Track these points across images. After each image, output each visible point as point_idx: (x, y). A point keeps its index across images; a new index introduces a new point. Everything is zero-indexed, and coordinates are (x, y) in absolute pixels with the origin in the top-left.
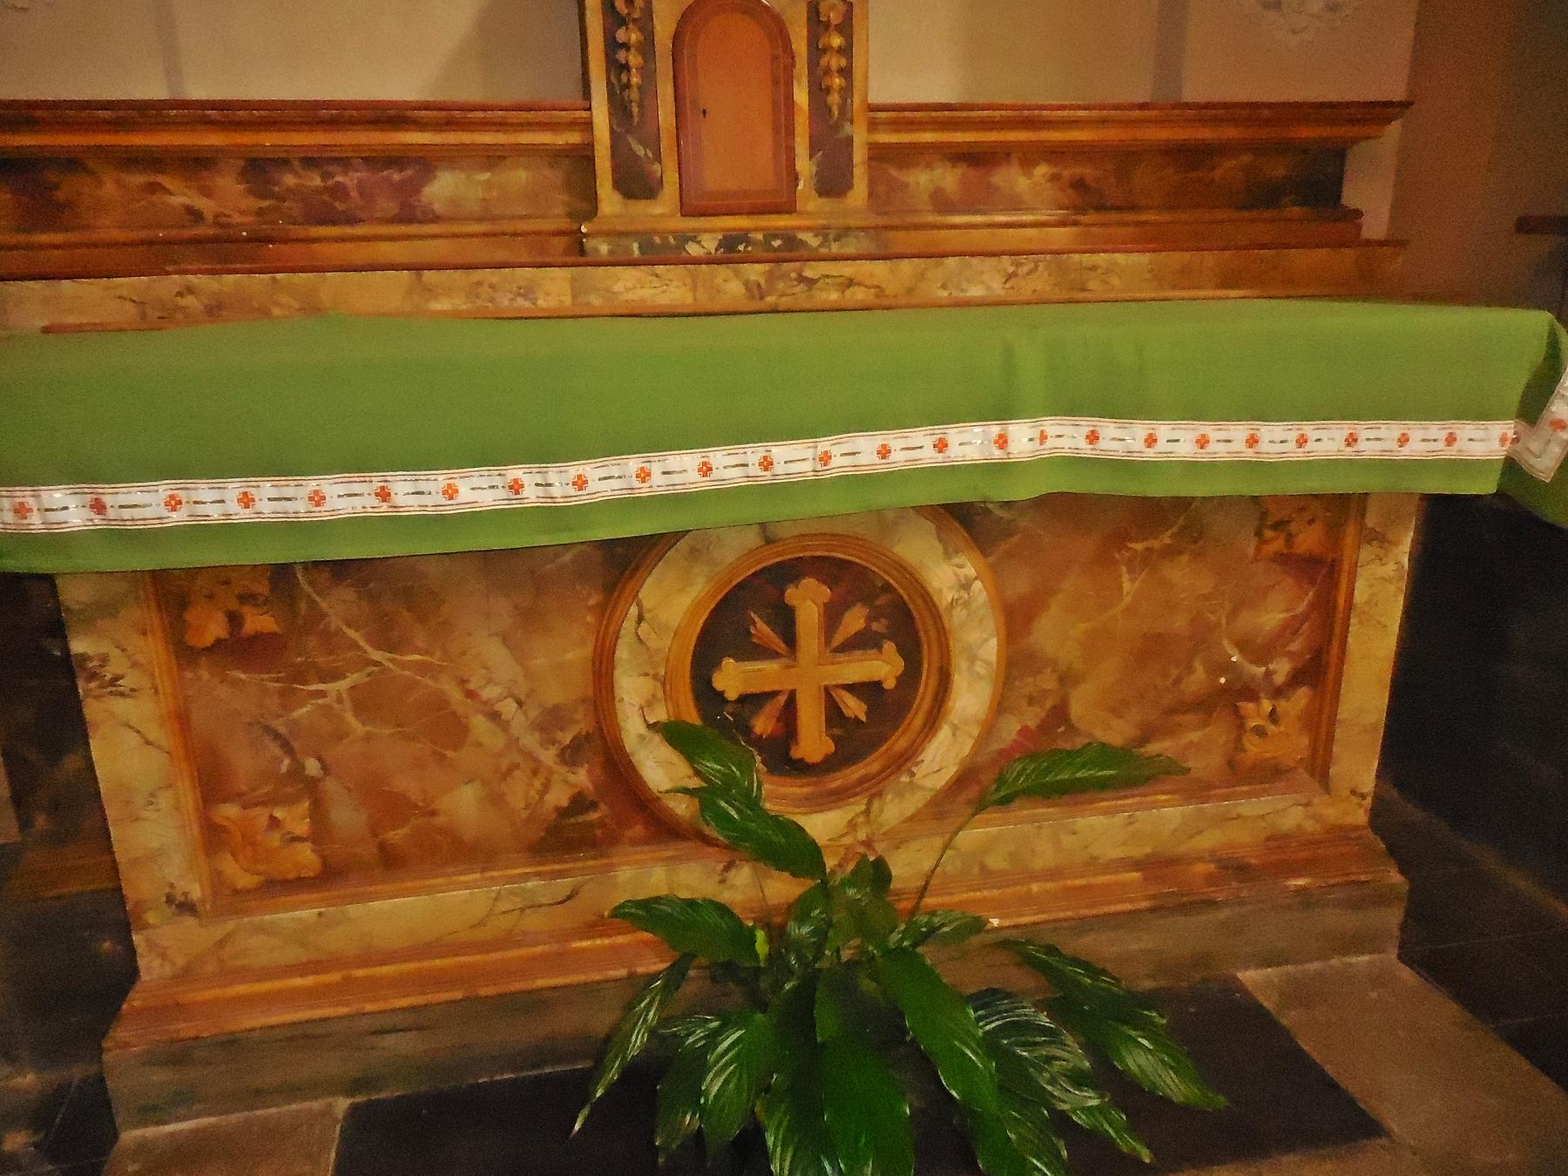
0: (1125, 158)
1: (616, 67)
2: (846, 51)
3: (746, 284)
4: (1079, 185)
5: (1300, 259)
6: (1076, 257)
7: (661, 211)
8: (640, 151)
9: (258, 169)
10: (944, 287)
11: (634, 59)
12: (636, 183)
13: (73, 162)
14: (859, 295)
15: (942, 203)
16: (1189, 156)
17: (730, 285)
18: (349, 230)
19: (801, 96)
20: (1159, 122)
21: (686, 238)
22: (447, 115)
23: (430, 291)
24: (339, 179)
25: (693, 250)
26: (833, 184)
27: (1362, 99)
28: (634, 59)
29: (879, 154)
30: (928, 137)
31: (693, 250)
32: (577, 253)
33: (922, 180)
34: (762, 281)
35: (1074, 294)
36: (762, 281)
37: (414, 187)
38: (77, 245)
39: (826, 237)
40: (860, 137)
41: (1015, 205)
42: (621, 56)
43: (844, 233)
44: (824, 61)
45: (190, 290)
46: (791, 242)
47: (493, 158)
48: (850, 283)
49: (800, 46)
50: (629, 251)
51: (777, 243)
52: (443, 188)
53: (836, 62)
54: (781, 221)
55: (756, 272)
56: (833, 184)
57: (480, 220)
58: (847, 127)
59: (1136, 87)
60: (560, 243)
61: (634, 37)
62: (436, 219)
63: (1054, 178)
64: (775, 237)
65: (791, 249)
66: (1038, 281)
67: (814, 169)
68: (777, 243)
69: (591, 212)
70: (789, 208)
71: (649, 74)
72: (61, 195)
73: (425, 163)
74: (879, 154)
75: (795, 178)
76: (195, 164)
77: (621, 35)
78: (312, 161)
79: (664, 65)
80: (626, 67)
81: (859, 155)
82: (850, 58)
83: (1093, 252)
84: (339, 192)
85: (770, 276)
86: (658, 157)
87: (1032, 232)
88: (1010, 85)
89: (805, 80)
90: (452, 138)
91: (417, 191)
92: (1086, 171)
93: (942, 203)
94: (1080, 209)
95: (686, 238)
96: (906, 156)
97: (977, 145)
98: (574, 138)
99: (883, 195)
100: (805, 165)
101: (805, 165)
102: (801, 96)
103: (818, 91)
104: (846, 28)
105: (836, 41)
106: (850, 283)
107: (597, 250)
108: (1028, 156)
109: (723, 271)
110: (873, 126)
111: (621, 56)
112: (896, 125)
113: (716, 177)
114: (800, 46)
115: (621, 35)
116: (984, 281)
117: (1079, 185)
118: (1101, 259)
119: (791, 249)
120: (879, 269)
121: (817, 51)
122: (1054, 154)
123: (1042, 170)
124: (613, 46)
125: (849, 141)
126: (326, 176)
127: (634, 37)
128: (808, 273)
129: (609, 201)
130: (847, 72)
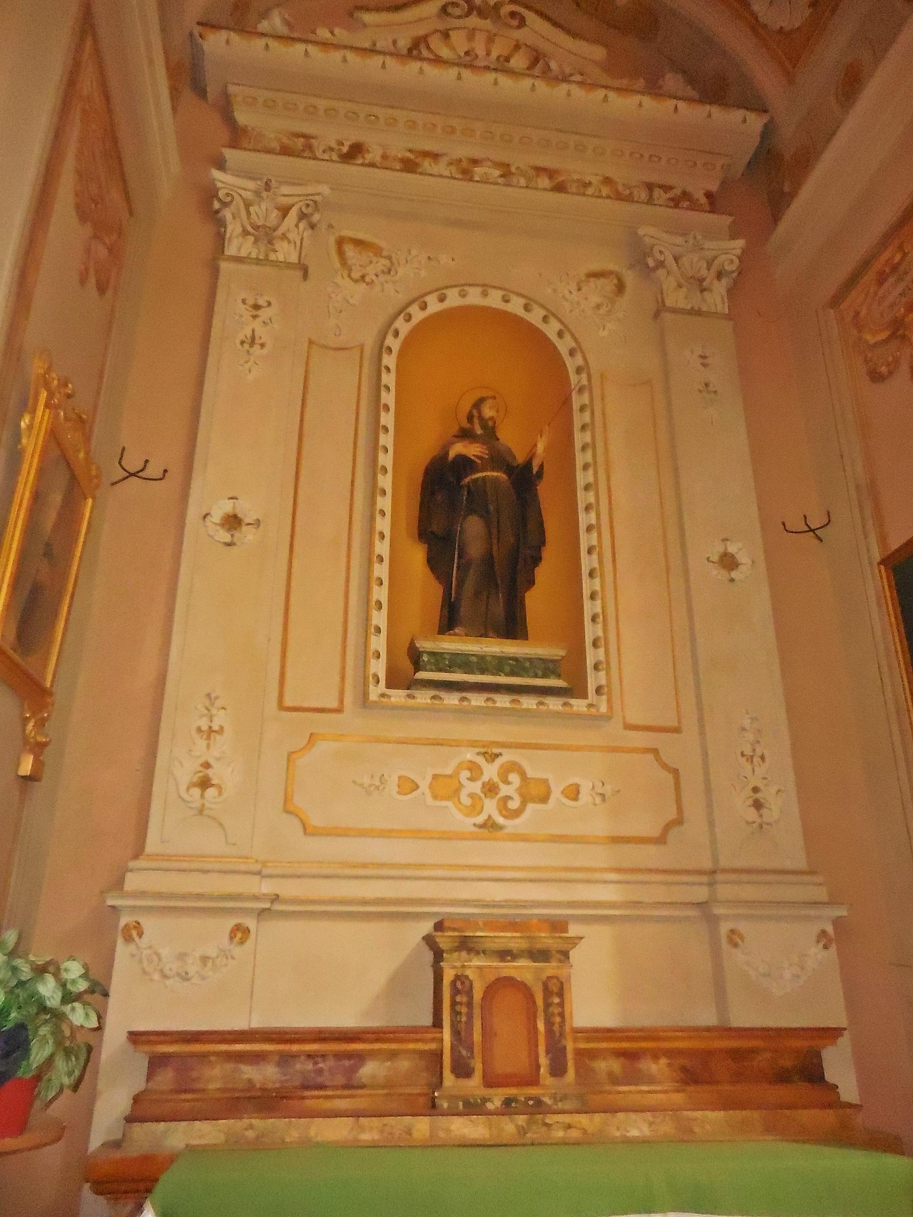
0: (707, 1055)
1: (455, 1013)
2: (561, 1005)
3: (517, 1126)
4: (684, 1069)
5: (806, 1116)
6: (685, 1113)
7: (474, 1085)
8: (464, 1052)
9: (285, 1059)
10: (618, 1129)
11: (464, 1010)
12: (462, 1070)
13: (203, 1057)
14: (574, 1134)
15: (614, 1080)
16: (736, 1055)
17: (509, 1127)
18: (322, 1093)
19: (541, 1026)
20: (683, 1039)
21: (485, 1100)
22: (378, 1035)
23: (362, 1129)
24: (320, 1065)
25: (490, 1106)
26: (558, 1070)
27: (811, 1026)
28: (464, 1010)
29: (579, 1053)
30: (604, 1045)
31: (490, 1106)
32: (432, 1108)
33: (602, 1066)
34: (524, 1124)
35: (685, 1135)
36: (524, 1124)
37: (353, 1070)
38: (198, 1100)
39: (555, 1098)
40: (570, 1046)
41: (651, 1080)
42: (458, 1008)
43: (564, 1098)
44: (551, 1009)
45: (251, 1127)
46: (539, 1102)
47: (393, 1055)
48: (569, 1127)
49: (540, 1002)
50: (458, 1107)
51: (531, 1102)
52: (370, 1070)
53: (556, 1010)
54: (532, 1091)
55: (521, 1119)
56: (558, 1070)
57: (383, 1087)
58: (564, 1042)
59: (707, 1017)
60: (422, 1100)
61: (465, 999)
62: (362, 1087)
63: (669, 1065)
64: (531, 1099)
65: (537, 1107)
66: (667, 1127)
67: (548, 1062)
68: (531, 1102)
69: (439, 1083)
70: (534, 1081)
71: (470, 1016)
72: (194, 1074)
73: (360, 1058)
74: (579, 1053)
75: (538, 1067)
76: (257, 1058)
77: (458, 999)
78: (310, 1056)
79: (477, 1012)
80: (460, 1013)
81: (570, 1056)
82: (563, 1007)
83: (693, 1110)
84: (320, 1072)
85: (529, 1123)
86: (472, 1057)
87: (660, 1096)
88: (645, 1017)
89: (542, 1018)
90: (377, 1046)
91: (357, 1071)
92: (682, 1061)
93: (614, 1080)
94: (687, 1083)
95: (485, 1100)
96: (593, 1054)
97: (629, 1048)
98: (433, 1046)
99: (584, 1073)
100: (544, 1060)
101: (544, 1060)
102: (541, 1026)
103: (549, 1023)
104: (561, 994)
105: (556, 1000)
106: (569, 1127)
107: (442, 1106)
108: (655, 1055)
109: (505, 1119)
110: (575, 1040)
111: (458, 1008)
112: (588, 1040)
113: (502, 1067)
114: (540, 1002)
115: (458, 999)
116: (637, 1127)
117: (684, 1069)
118: (698, 1114)
119: (537, 1107)
120: (583, 1120)
121: (547, 1005)
122: (670, 1054)
123: (663, 1061)
124: (454, 1003)
125: (565, 1048)
126: (316, 1063)
127: (465, 999)
128: (548, 1121)
129: (449, 1078)
130: (562, 1014)
